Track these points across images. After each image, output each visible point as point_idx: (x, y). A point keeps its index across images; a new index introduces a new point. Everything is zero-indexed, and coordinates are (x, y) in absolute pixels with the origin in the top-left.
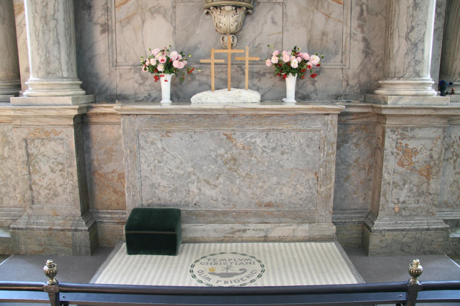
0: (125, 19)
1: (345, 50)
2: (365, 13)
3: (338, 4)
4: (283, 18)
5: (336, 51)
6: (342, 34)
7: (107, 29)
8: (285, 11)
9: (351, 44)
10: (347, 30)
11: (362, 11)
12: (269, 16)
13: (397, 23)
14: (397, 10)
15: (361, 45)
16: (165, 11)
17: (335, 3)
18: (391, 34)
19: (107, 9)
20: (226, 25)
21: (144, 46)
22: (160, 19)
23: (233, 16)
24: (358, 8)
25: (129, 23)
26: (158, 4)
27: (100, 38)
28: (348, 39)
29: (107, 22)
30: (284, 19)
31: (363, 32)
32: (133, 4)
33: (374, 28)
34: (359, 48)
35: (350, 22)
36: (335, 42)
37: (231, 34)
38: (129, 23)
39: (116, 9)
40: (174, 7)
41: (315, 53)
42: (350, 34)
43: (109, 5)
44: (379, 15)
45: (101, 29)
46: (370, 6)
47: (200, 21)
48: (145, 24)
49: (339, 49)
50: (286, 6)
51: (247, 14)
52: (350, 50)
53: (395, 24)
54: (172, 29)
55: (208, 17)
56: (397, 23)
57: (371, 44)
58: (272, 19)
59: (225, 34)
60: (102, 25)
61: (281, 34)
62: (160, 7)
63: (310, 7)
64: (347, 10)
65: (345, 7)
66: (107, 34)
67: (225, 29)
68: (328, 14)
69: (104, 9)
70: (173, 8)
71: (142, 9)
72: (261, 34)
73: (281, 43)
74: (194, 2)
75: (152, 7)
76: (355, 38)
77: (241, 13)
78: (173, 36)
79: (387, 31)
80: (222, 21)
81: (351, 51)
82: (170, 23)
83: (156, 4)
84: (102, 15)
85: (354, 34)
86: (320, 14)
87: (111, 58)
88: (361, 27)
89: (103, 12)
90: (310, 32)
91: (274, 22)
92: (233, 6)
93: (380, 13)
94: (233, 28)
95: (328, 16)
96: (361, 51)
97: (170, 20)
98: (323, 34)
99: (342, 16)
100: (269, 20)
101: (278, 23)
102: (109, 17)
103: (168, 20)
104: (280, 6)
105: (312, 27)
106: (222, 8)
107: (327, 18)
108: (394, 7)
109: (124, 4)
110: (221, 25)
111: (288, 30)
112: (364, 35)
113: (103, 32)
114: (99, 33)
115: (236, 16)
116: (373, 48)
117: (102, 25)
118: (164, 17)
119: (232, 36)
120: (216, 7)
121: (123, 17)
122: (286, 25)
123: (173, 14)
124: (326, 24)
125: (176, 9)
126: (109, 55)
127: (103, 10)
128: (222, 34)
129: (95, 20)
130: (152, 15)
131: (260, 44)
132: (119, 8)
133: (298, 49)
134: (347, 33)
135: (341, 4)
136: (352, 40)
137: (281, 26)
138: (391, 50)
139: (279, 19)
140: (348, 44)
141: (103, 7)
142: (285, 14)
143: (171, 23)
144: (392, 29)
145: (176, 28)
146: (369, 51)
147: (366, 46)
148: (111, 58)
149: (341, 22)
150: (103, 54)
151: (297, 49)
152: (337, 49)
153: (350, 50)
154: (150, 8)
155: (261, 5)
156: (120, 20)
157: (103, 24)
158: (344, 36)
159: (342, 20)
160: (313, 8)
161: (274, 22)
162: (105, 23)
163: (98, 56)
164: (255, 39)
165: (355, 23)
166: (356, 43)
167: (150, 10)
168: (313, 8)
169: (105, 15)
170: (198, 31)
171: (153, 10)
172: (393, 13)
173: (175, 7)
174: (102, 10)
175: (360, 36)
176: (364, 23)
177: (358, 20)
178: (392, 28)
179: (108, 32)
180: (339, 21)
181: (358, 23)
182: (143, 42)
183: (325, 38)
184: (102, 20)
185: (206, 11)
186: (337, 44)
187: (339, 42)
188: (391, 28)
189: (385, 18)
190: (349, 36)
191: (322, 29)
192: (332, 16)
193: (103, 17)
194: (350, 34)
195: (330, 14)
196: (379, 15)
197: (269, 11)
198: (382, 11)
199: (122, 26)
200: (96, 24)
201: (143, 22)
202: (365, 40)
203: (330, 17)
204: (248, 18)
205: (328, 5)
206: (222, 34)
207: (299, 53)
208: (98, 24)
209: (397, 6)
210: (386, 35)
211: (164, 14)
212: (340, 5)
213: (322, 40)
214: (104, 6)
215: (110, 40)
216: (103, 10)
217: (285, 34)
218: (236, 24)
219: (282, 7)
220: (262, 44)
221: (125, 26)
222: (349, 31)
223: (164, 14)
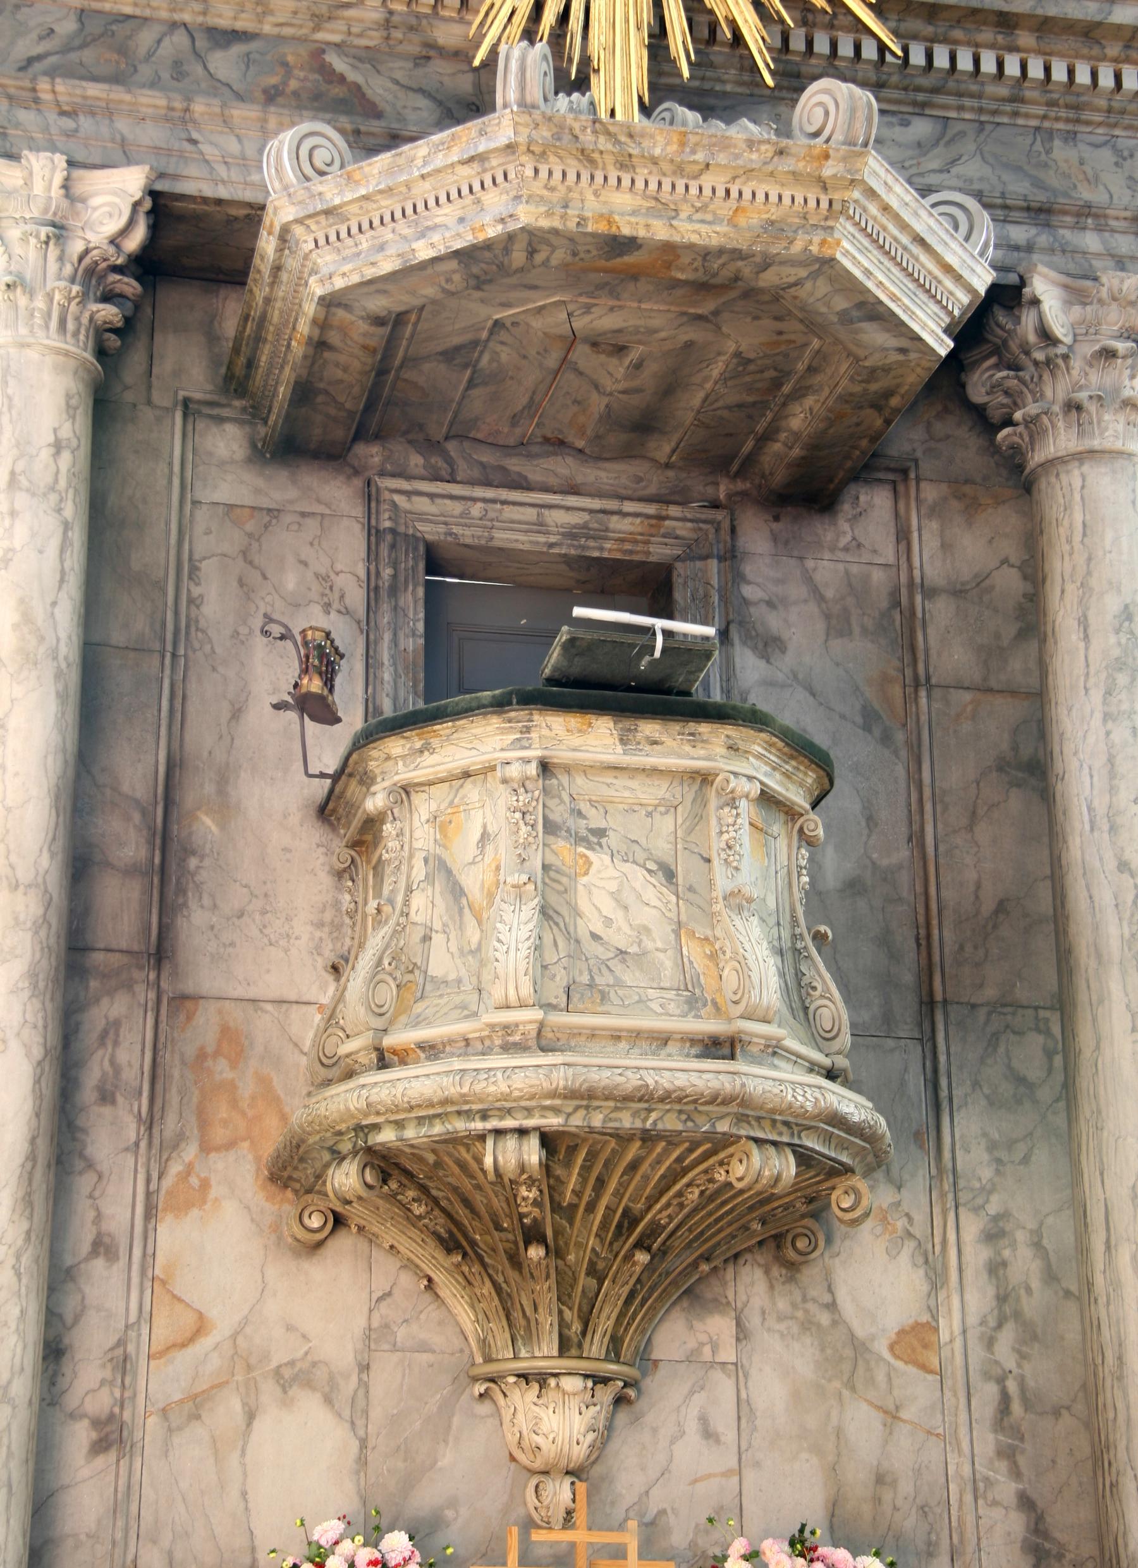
0: (182, 1401)
1: (961, 1541)
2: (1016, 1407)
3: (922, 1374)
4: (739, 1418)
5: (929, 1543)
6: (943, 1480)
7: (115, 1436)
8: (743, 1395)
9: (978, 1518)
10: (961, 1467)
11: (1005, 1399)
12: (693, 1412)
13: (1127, 1448)
14: (1120, 1405)
15: (1016, 1523)
16: (331, 1379)
17: (911, 1370)
18: (1112, 1485)
19: (125, 1360)
20: (559, 1441)
21: (247, 1509)
22: (310, 1406)
23: (584, 1408)
24: (991, 1390)
25: (198, 1417)
26: (306, 1354)
27: (85, 1472)
28: (969, 1498)
29: (117, 1410)
30: (743, 1421)
31: (1016, 1473)
32: (217, 1346)
33: (1053, 1461)
34: (1009, 1534)
35: (968, 1438)
36: (922, 1508)
37: (567, 1473)
38: (198, 1417)
39: (152, 1363)
40: (365, 1368)
41: (870, 1547)
42: (975, 1481)
43: (131, 1348)
44: (1064, 1412)
45: (94, 1435)
46: (1031, 1383)
47: (456, 1421)
48: (256, 1424)
49: (938, 1535)
50: (746, 1376)
51: (620, 1401)
52: (979, 1539)
53: (1122, 1455)
54: (355, 1445)
55: (485, 1408)
56: (1127, 1448)
57: (1048, 1519)
58: (703, 1420)
59: (546, 1473)
60: (96, 1423)
61: (736, 1479)
62: (314, 1364)
63: (830, 1380)
64: (955, 1395)
65: (948, 1383)
66: (112, 1455)
67: (552, 1455)
68: (891, 1407)
69: (111, 1360)
70: (361, 1372)
71: (249, 1368)
72: (666, 1476)
73: (737, 1511)
74: (434, 1352)
75: (286, 1365)
76: (990, 1497)
77: (606, 1395)
78: (357, 1472)
79: (1099, 1473)
80: (544, 1427)
81: (984, 1543)
82: (347, 1425)
83: (301, 1352)
84: (103, 1382)
85: (987, 1479)
86: (864, 1406)
87: (118, 1551)
88: (1008, 1454)
89: (107, 1374)
90: (833, 1470)
91: (709, 1434)
92: (586, 1376)
93: (1068, 1408)
94: (579, 1453)
95: (891, 1416)
96: (1019, 1545)
97: (347, 1413)
98: (881, 1479)
99: (939, 1416)
100: (692, 1426)
101: (723, 1438)
102: (127, 1394)
103: (340, 1415)
104: (729, 1376)
105: (839, 1455)
106: (552, 1382)
107: (889, 1420)
108: (1109, 1395)
109: (183, 1345)
110: (539, 1440)
111: (757, 1464)
112: (1021, 1487)
113: (100, 1446)
114: (85, 1450)
115: (593, 1410)
116: (1057, 1535)
117: (96, 1423)
118: (328, 1400)
119: (568, 1480)
120: (524, 1377)
121: (177, 1397)
122: (750, 1446)
123: (361, 1393)
124: (886, 1442)
125: (372, 1374)
126: (114, 1543)
127: (109, 1365)
128: (534, 1473)
129: (72, 1401)
130: (285, 1392)
131: (662, 1512)
132: (162, 1360)
133: (813, 1533)
134: (962, 1478)
135: (931, 1372)
136: (980, 1502)
137: (736, 1449)
138: (1120, 1541)
139: (724, 1421)
140: (970, 1519)
141: (109, 1356)
142: (744, 1406)
143: (353, 1423)
144: (1114, 1470)
145: (370, 1445)
146: (1047, 1545)
147: (1032, 1526)
148: (118, 1551)
149: (938, 1435)
150: (88, 1535)
151: (807, 1534)
152: (934, 1537)
153: (979, 1539)
154: (279, 1367)
155: (663, 1371)
156: (161, 1405)
157: (103, 1417)
158: (951, 1486)
159: (940, 1431)
160: (837, 1384)
161: (709, 1434)
162: (111, 1417)
163: (70, 1542)
164: (647, 1492)
165: (987, 1442)
166: (997, 1513)
167: (277, 1372)
168: (837, 1384)
169: (112, 1383)
170: (446, 1458)
171: (287, 1373)
172: (1111, 1415)
173: (368, 1367)
174: (104, 1366)
175: (1007, 1489)
176: (1016, 1443)
177: (995, 1431)
178: (1114, 1466)
179: (119, 1451)
180: (929, 1433)
181: (997, 1440)
182: (244, 1494)
183: (887, 1496)
184: (100, 1403)
185: (480, 1388)
186: (930, 1518)
187: (938, 1510)
188: (1110, 1464)
189: (1087, 1425)
190: (969, 1488)
191: (875, 1463)
192: (904, 1415)
193: (105, 1390)
194: (975, 1481)
195: (897, 1408)
196: (1064, 1412)
197: (692, 1393)
198: (1074, 1401)
199: (170, 1430)
200: (73, 1416)
201: (251, 1416)
202: (1026, 1502)
203: (899, 1418)
204: (622, 1416)
205: (889, 1376)
206: (534, 1473)
207: (815, 1549)
208: (85, 1415)
209: (1118, 1393)
210: (1097, 1489)
211: (327, 1389)
212: (930, 1377)
213: (877, 1500)
214: (112, 1349)
215: (122, 1482)
216: (109, 1366)
217: (749, 1476)
218: (591, 1436)
219: (734, 1379)
220: (669, 1511)
221: (180, 1429)
222: (967, 1470)
223: (327, 1389)
